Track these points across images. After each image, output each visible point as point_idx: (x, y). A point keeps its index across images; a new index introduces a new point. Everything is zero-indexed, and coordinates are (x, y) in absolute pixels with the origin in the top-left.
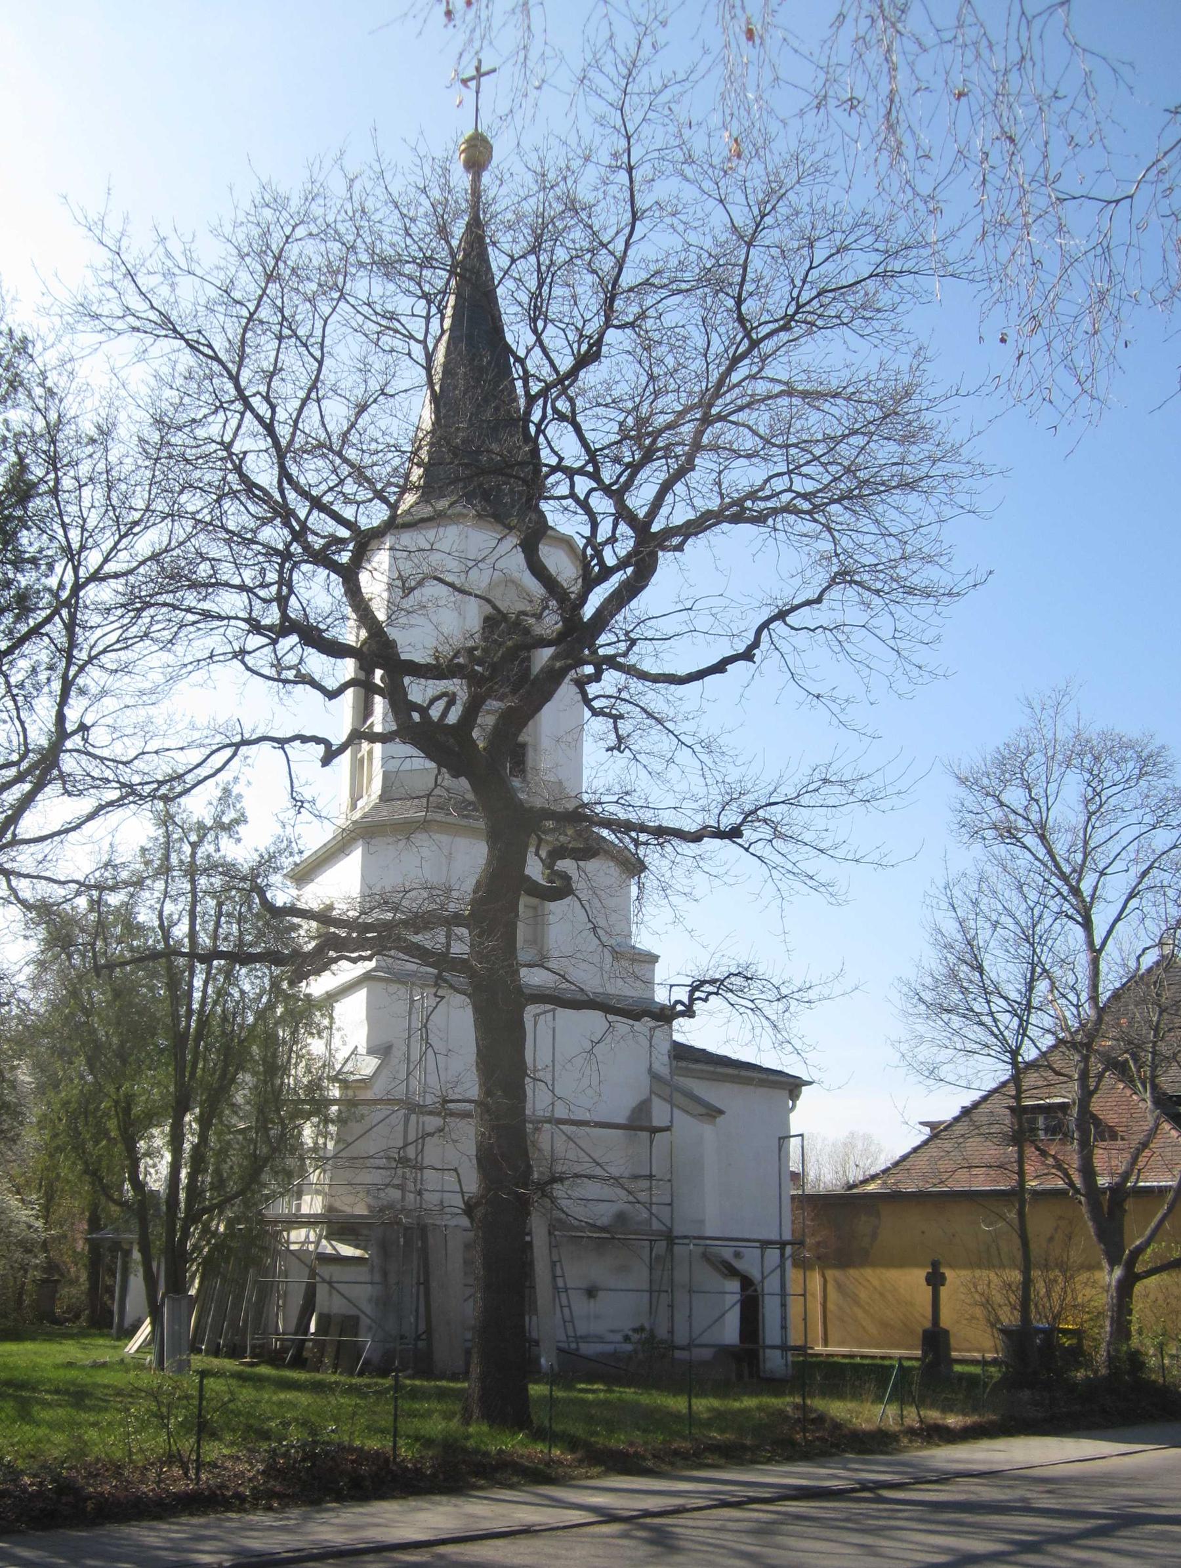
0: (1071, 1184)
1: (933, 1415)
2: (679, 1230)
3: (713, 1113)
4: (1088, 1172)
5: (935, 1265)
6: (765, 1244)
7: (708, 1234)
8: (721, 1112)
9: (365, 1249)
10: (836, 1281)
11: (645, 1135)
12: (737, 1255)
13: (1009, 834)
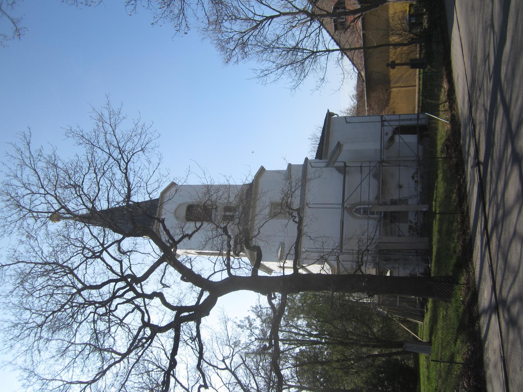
0: (359, 17)
1: (443, 96)
2: (378, 159)
3: (339, 146)
4: (354, 12)
5: (388, 65)
6: (383, 125)
7: (380, 148)
8: (339, 143)
9: (387, 271)
10: (395, 83)
11: (347, 168)
12: (387, 134)
13: (244, 45)
